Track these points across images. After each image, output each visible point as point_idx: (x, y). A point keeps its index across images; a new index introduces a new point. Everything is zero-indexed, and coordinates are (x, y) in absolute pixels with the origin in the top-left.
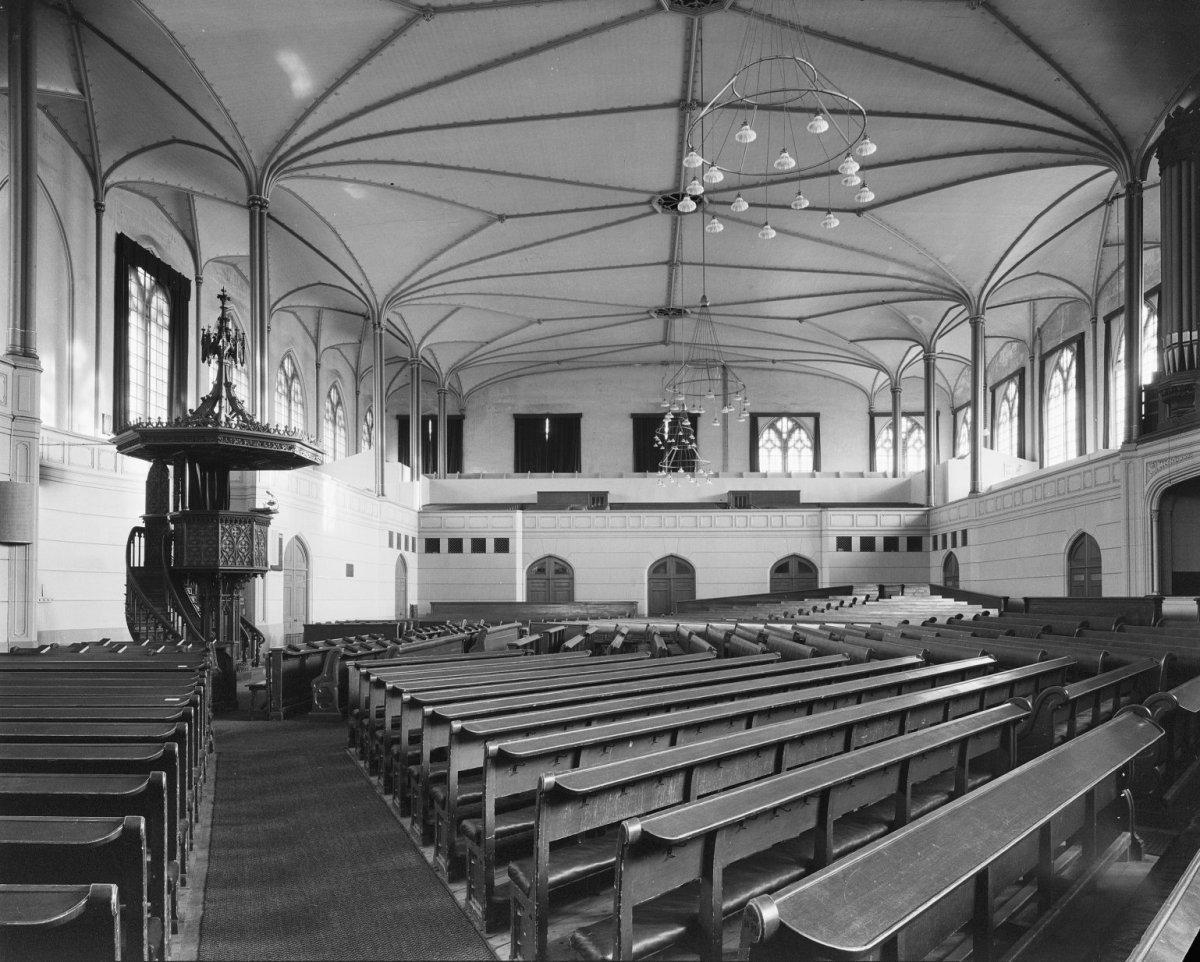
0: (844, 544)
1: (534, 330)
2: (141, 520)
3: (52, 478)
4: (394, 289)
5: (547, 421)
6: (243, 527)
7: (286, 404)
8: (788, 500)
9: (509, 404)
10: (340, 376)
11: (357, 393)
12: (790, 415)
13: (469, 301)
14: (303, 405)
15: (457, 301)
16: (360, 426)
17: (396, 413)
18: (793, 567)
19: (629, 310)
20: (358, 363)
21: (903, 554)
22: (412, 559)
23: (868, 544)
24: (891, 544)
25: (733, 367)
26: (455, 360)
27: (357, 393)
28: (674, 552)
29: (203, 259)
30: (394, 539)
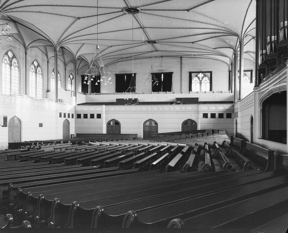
0: (205, 116)
1: (111, 49)
4: (59, 40)
5: (162, 75)
8: (194, 101)
9: (114, 71)
11: (65, 69)
12: (202, 72)
13: (86, 42)
17: (81, 75)
18: (189, 123)
19: (120, 43)
21: (225, 120)
23: (213, 116)
24: (221, 116)
25: (184, 57)
27: (65, 69)
28: (190, 118)
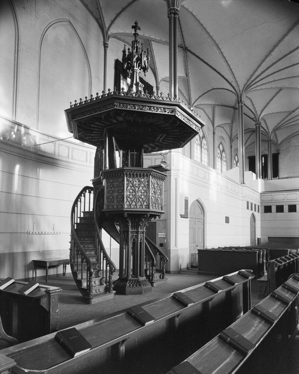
2: (91, 182)
3: (58, 165)
6: (143, 180)
7: (200, 149)
10: (223, 139)
14: (208, 150)
15: (279, 85)
16: (232, 162)
20: (231, 133)
22: (258, 216)
26: (275, 125)
27: (231, 147)
29: (160, 79)
30: (249, 206)
